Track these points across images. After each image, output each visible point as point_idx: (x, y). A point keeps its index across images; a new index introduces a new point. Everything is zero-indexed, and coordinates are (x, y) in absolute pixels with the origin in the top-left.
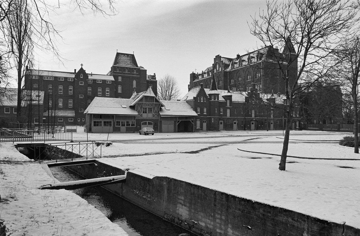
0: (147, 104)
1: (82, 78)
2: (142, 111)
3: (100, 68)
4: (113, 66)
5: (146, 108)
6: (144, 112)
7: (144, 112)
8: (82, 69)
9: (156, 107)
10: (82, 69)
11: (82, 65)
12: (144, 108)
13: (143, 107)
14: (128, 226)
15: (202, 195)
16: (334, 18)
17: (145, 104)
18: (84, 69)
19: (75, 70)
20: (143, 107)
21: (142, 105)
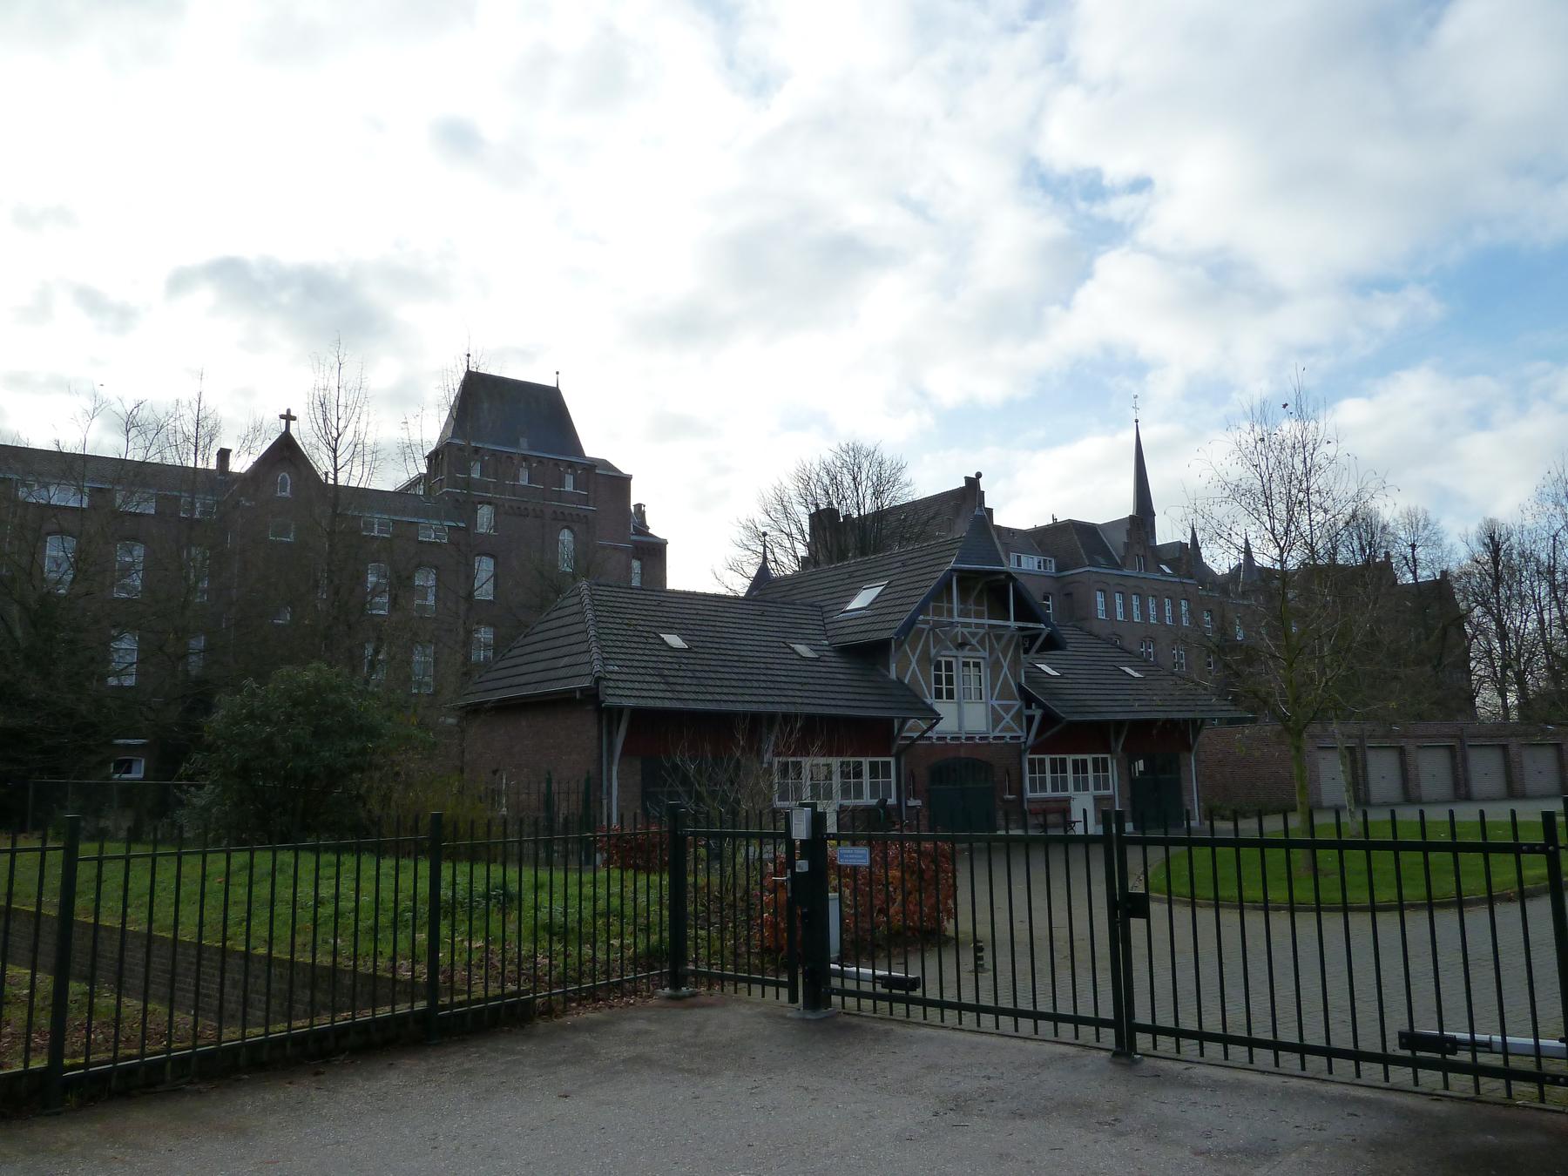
5: (949, 666)
12: (938, 667)
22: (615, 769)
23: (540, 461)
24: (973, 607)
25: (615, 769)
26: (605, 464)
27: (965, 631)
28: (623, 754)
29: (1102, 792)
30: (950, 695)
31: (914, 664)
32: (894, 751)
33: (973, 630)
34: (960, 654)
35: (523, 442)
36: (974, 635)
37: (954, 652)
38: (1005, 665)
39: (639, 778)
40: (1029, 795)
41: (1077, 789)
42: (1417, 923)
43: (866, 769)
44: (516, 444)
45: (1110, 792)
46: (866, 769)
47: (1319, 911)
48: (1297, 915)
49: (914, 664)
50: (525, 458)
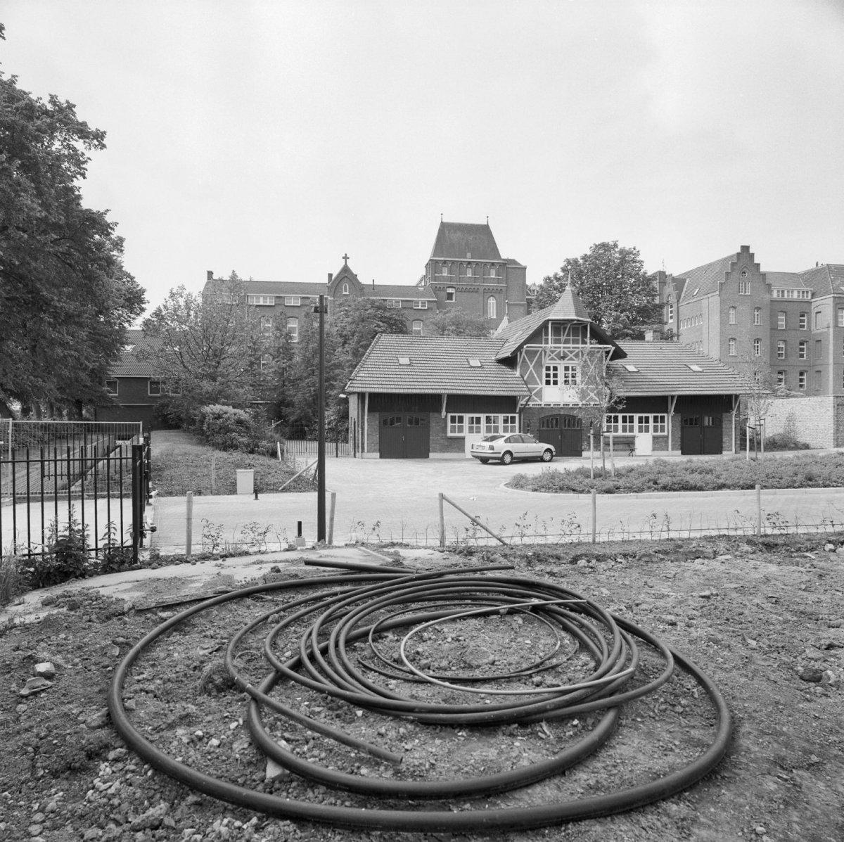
0: (578, 353)
1: (347, 293)
2: (541, 380)
3: (398, 263)
4: (430, 260)
5: (555, 369)
6: (548, 383)
7: (548, 383)
8: (346, 269)
9: (531, 362)
10: (346, 269)
11: (346, 258)
12: (548, 369)
13: (547, 362)
14: (123, 264)
15: (207, 420)
16: (52, 465)
17: (552, 352)
18: (355, 273)
19: (330, 275)
20: (547, 362)
21: (541, 354)
22: (366, 417)
23: (477, 264)
24: (571, 338)
25: (366, 417)
26: (514, 262)
27: (566, 350)
28: (369, 411)
29: (659, 434)
30: (555, 383)
31: (531, 368)
32: (517, 411)
33: (571, 349)
34: (562, 362)
35: (469, 255)
36: (571, 352)
37: (558, 361)
38: (531, 366)
39: (377, 422)
40: (449, 434)
41: (640, 431)
42: (35, 506)
43: (620, 419)
44: (465, 257)
45: (666, 433)
46: (620, 419)
47: (96, 498)
48: (123, 500)
49: (531, 368)
50: (469, 263)
